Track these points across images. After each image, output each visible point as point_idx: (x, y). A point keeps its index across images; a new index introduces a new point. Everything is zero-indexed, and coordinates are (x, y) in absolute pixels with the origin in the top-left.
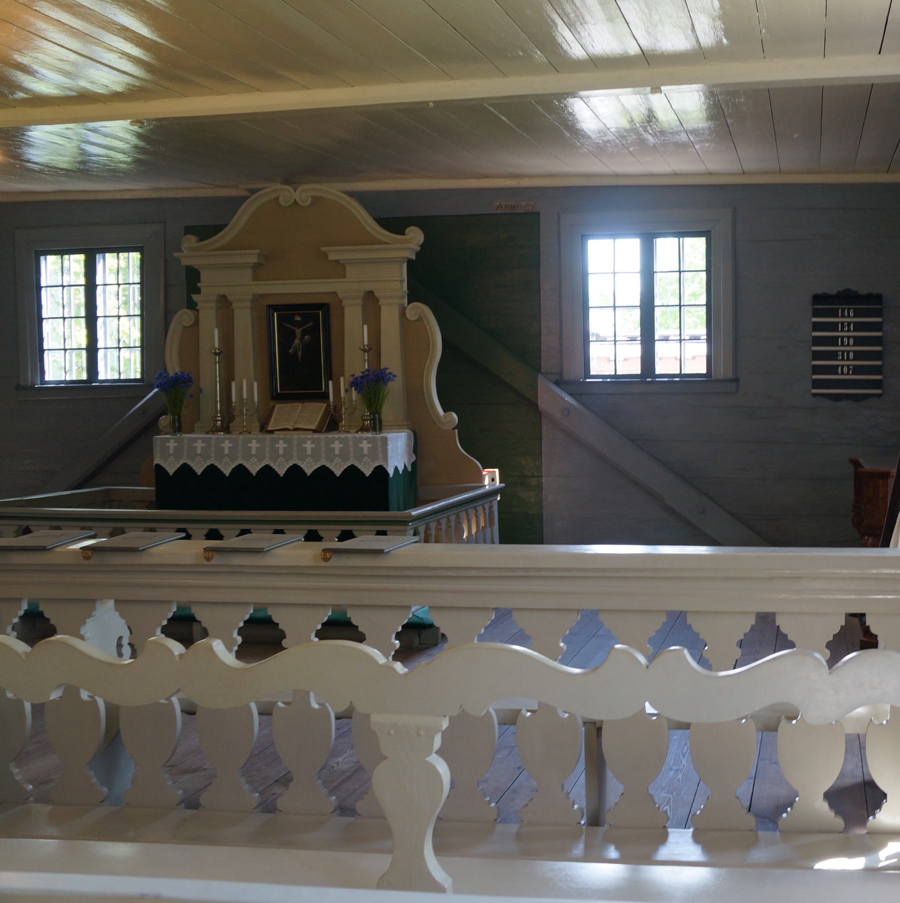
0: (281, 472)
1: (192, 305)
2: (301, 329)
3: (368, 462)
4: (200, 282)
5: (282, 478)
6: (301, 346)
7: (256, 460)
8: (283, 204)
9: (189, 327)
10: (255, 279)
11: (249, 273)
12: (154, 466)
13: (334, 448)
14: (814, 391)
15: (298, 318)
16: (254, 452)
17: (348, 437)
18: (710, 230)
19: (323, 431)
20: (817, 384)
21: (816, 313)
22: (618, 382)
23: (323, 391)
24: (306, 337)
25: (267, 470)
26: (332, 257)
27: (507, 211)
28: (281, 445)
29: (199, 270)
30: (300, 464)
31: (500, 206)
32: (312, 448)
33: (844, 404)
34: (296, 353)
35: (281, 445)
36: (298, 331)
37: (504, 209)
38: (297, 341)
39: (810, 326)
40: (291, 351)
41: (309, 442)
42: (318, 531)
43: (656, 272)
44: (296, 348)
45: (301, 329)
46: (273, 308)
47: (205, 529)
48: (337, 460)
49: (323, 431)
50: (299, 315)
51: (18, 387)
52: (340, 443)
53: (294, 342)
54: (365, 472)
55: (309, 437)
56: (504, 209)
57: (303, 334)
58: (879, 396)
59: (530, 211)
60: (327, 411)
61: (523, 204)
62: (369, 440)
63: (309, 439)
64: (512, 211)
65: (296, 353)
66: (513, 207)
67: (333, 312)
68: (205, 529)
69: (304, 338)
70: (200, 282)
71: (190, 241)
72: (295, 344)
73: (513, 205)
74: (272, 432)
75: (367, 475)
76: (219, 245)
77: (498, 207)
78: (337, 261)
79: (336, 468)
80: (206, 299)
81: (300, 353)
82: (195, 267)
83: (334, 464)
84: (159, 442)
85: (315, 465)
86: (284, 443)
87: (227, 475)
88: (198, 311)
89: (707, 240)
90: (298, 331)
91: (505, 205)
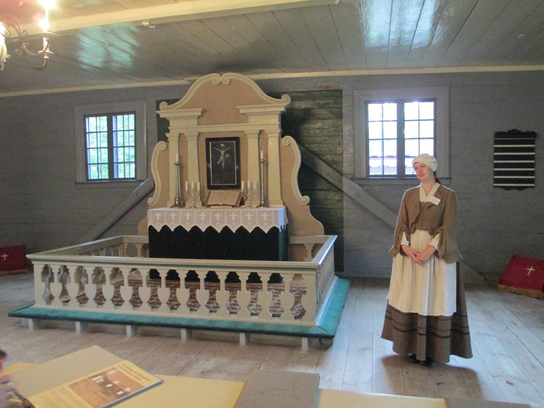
0: (203, 230)
1: (166, 139)
2: (224, 151)
3: (266, 225)
4: (169, 127)
5: (235, 233)
6: (224, 160)
7: (204, 223)
8: (214, 84)
9: (164, 151)
10: (198, 124)
12: (148, 227)
13: (247, 217)
14: (495, 185)
15: (222, 145)
16: (203, 219)
17: (256, 211)
18: (436, 97)
19: (238, 206)
20: (496, 181)
21: (496, 142)
22: (384, 179)
23: (236, 184)
24: (227, 155)
25: (241, 230)
26: (242, 111)
28: (218, 216)
30: (168, 225)
32: (251, 217)
33: (512, 192)
34: (221, 163)
35: (218, 216)
36: (223, 152)
38: (222, 158)
39: (493, 150)
40: (218, 163)
41: (233, 213)
43: (90, 164)
45: (224, 151)
46: (208, 140)
48: (173, 223)
49: (238, 206)
50: (224, 143)
51: (76, 183)
52: (267, 214)
53: (220, 158)
54: (248, 231)
55: (203, 210)
57: (225, 154)
58: (532, 187)
60: (240, 195)
62: (190, 212)
63: (233, 212)
64: (327, 89)
65: (221, 163)
66: (328, 87)
67: (242, 141)
69: (225, 156)
70: (169, 127)
71: (163, 105)
72: (220, 159)
74: (209, 206)
75: (250, 232)
76: (179, 107)
78: (244, 114)
79: (265, 228)
80: (172, 136)
81: (223, 164)
82: (167, 119)
83: (232, 225)
84: (151, 213)
85: (176, 225)
86: (160, 214)
87: (219, 232)
88: (168, 142)
89: (434, 104)
90: (223, 152)
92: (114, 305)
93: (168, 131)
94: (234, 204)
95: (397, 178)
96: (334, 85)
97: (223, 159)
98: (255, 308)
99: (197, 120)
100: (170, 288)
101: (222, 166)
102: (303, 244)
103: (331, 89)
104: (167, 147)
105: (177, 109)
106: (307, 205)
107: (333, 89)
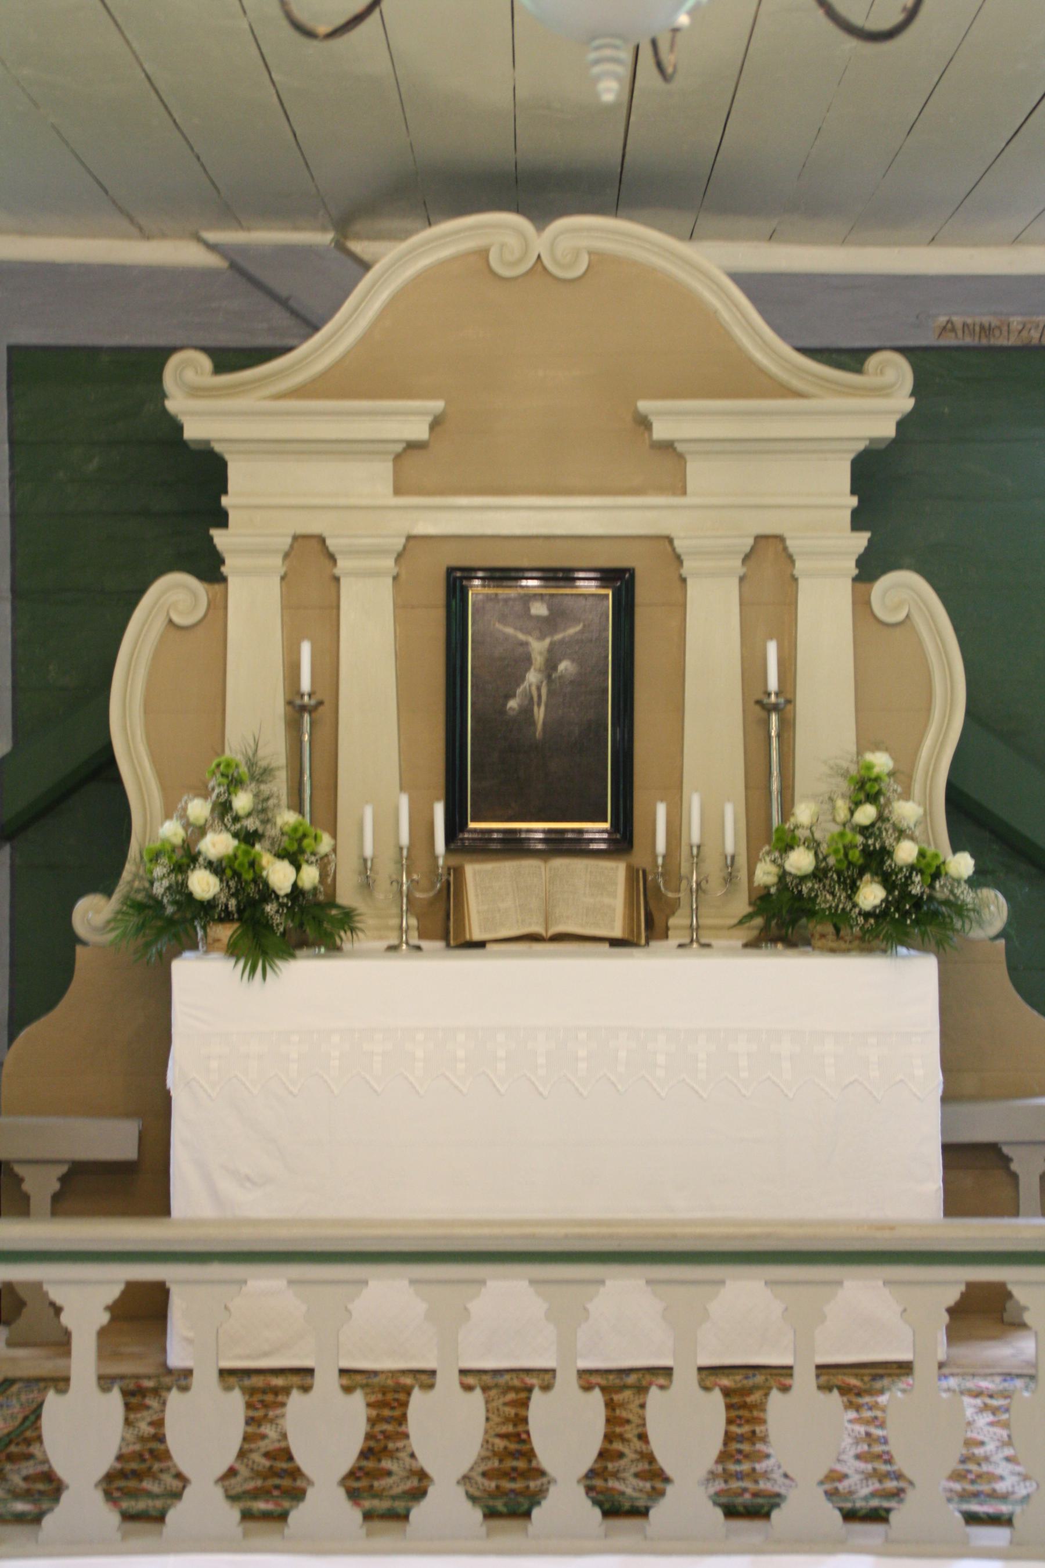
6: (544, 691)
11: (385, 469)
26: (661, 431)
27: (968, 341)
29: (227, 457)
31: (949, 325)
34: (527, 711)
37: (960, 333)
38: (533, 677)
40: (513, 704)
42: (46, 1287)
44: (532, 698)
45: (547, 641)
47: (111, 1282)
53: (523, 678)
56: (960, 333)
59: (1035, 341)
61: (1016, 321)
64: (984, 342)
65: (527, 711)
66: (986, 330)
68: (111, 1282)
69: (555, 668)
72: (526, 684)
73: (987, 325)
77: (944, 328)
81: (540, 714)
91: (965, 325)
92: (357, 1515)
93: (221, 519)
94: (617, 933)
95: (435, 858)
96: (1016, 321)
97: (539, 689)
98: (251, 1485)
99: (390, 465)
100: (244, 1390)
101: (531, 721)
102: (993, 1148)
103: (1002, 342)
104: (219, 608)
105: (265, 398)
106: (997, 937)
107: (1013, 341)
